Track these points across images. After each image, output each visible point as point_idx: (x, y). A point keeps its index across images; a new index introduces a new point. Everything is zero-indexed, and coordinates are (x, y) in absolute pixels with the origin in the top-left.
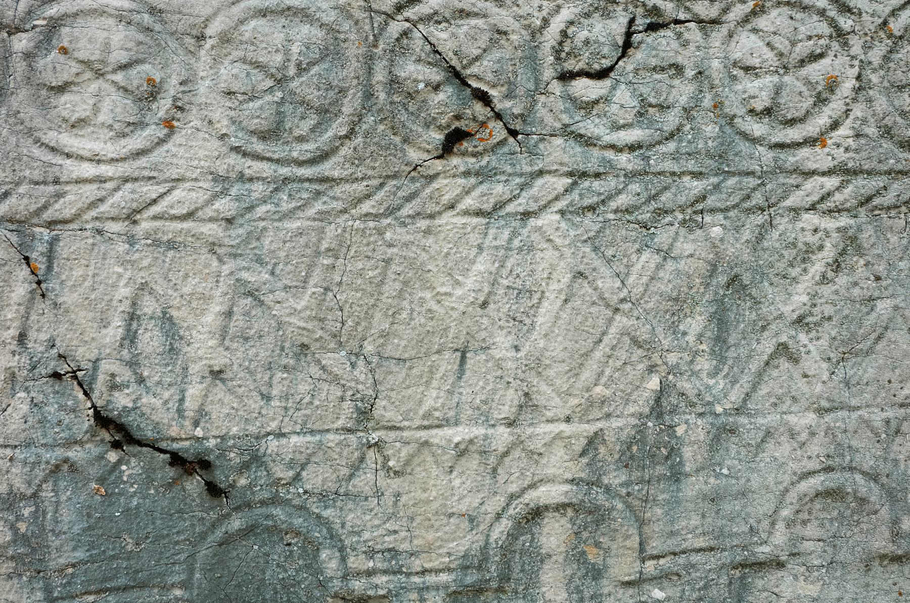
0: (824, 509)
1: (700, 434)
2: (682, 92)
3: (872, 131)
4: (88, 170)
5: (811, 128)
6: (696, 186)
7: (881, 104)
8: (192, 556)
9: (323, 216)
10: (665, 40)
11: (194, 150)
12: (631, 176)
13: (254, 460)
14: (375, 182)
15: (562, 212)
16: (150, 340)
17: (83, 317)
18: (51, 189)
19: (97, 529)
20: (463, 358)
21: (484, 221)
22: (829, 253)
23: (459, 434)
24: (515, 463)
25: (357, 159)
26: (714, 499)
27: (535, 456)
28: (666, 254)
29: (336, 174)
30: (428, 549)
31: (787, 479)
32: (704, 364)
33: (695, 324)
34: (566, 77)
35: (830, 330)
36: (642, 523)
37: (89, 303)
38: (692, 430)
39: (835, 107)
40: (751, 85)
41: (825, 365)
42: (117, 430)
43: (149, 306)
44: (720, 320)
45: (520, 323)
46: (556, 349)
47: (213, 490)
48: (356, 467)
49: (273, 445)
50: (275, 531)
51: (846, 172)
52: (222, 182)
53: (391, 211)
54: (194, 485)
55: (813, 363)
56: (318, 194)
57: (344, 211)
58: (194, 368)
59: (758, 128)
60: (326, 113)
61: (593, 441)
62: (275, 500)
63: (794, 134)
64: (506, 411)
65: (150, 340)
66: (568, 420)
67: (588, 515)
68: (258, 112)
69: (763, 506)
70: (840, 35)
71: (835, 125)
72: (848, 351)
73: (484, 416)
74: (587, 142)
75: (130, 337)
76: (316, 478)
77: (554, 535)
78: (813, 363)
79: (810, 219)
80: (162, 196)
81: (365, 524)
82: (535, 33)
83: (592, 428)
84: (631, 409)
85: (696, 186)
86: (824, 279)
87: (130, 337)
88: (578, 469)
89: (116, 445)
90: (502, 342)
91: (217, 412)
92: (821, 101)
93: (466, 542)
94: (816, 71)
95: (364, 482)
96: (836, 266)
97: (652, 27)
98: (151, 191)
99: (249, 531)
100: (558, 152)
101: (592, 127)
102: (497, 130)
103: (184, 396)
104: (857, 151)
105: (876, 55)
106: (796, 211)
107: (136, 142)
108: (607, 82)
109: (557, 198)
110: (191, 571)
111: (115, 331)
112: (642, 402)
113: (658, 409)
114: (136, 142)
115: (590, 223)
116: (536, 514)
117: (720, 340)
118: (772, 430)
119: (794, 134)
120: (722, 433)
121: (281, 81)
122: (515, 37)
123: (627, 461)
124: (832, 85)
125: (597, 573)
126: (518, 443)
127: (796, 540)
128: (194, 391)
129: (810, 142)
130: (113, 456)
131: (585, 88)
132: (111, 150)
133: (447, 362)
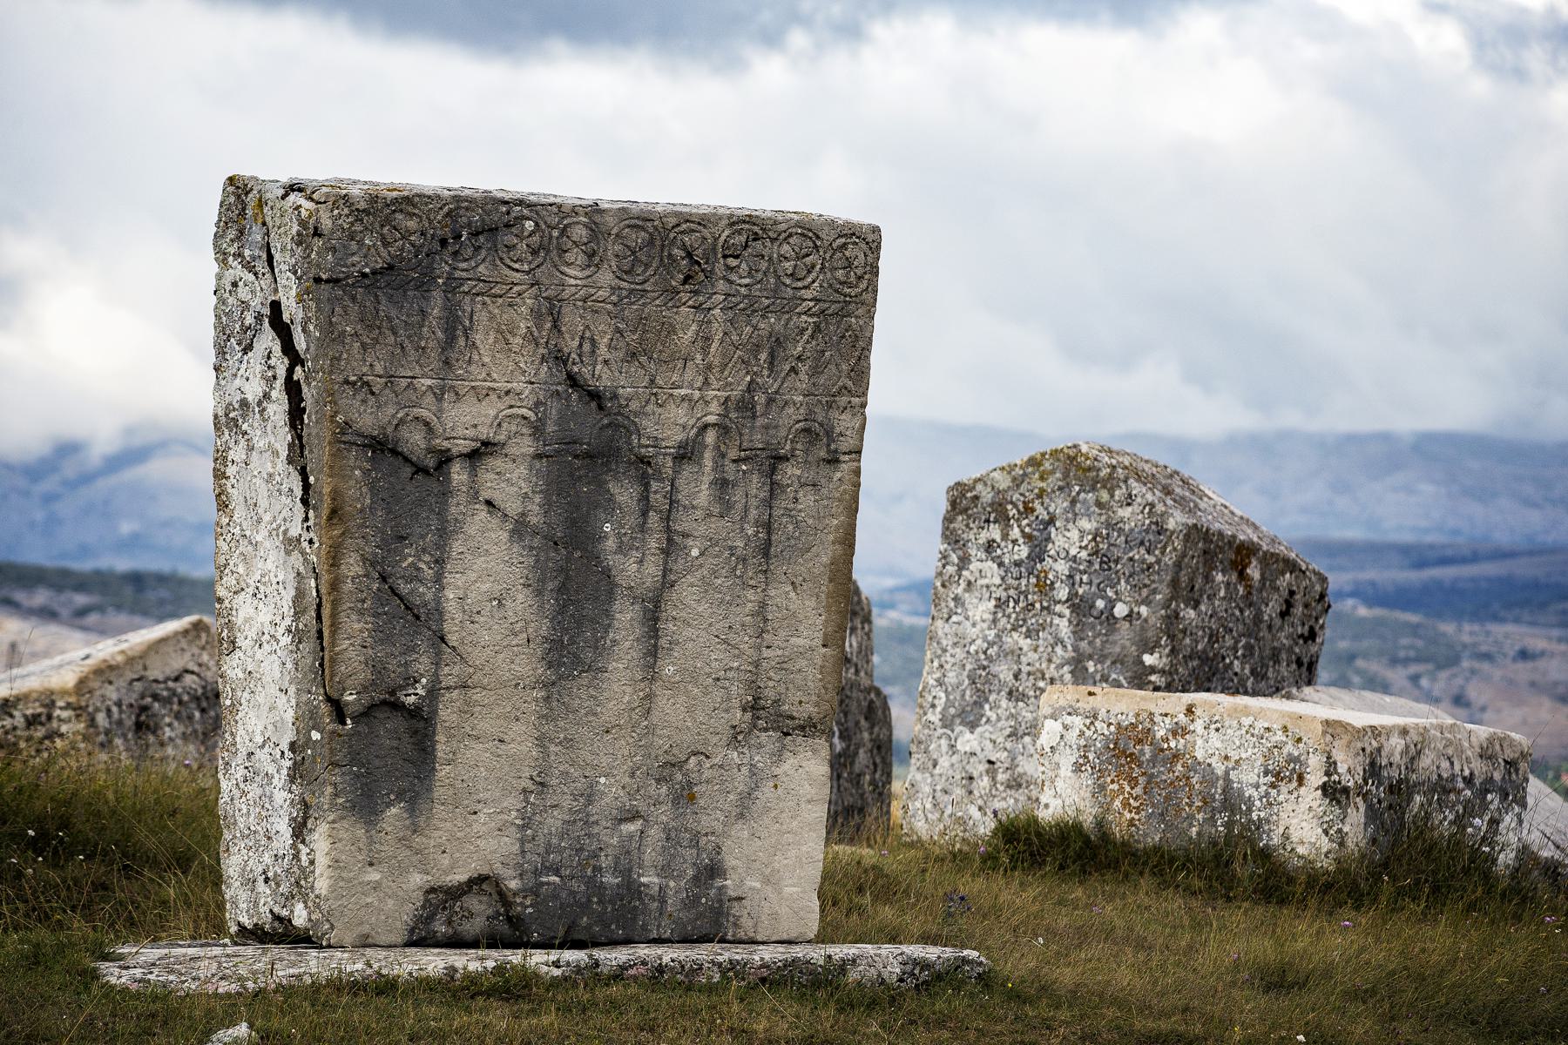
1: (763, 400)
2: (764, 265)
4: (573, 282)
5: (806, 283)
6: (767, 302)
7: (829, 275)
10: (758, 244)
12: (745, 296)
13: (615, 396)
16: (587, 347)
17: (567, 336)
19: (562, 420)
22: (809, 331)
23: (683, 392)
24: (700, 405)
25: (655, 284)
26: (766, 427)
27: (707, 403)
28: (755, 328)
30: (668, 438)
32: (766, 372)
33: (763, 356)
34: (725, 257)
35: (809, 362)
36: (741, 435)
37: (569, 332)
38: (760, 398)
39: (814, 274)
40: (787, 265)
42: (573, 381)
43: (588, 334)
44: (772, 355)
45: (705, 351)
46: (716, 362)
48: (647, 402)
49: (621, 391)
50: (618, 426)
54: (594, 405)
55: (803, 376)
59: (788, 281)
60: (647, 266)
61: (727, 399)
62: (619, 413)
63: (800, 284)
64: (699, 384)
65: (587, 347)
67: (723, 429)
68: (626, 266)
69: (783, 433)
70: (816, 247)
72: (815, 372)
73: (691, 387)
74: (731, 282)
75: (581, 345)
76: (634, 405)
77: (710, 437)
78: (803, 376)
81: (648, 425)
82: (716, 239)
85: (767, 302)
87: (581, 345)
88: (719, 410)
90: (699, 357)
91: (604, 376)
92: (809, 272)
93: (680, 437)
94: (808, 260)
95: (649, 408)
96: (812, 337)
99: (609, 425)
100: (721, 285)
101: (734, 277)
102: (701, 276)
103: (293, 426)
105: (827, 256)
107: (587, 273)
111: (576, 343)
112: (743, 387)
113: (749, 390)
114: (587, 273)
115: (730, 314)
116: (706, 426)
117: (771, 363)
118: (624, 861)
119: (800, 284)
120: (770, 401)
121: (634, 253)
123: (738, 409)
124: (813, 267)
125: (723, 456)
126: (702, 398)
127: (793, 450)
128: (599, 367)
129: (805, 287)
131: (732, 262)
132: (580, 275)
133: (680, 364)
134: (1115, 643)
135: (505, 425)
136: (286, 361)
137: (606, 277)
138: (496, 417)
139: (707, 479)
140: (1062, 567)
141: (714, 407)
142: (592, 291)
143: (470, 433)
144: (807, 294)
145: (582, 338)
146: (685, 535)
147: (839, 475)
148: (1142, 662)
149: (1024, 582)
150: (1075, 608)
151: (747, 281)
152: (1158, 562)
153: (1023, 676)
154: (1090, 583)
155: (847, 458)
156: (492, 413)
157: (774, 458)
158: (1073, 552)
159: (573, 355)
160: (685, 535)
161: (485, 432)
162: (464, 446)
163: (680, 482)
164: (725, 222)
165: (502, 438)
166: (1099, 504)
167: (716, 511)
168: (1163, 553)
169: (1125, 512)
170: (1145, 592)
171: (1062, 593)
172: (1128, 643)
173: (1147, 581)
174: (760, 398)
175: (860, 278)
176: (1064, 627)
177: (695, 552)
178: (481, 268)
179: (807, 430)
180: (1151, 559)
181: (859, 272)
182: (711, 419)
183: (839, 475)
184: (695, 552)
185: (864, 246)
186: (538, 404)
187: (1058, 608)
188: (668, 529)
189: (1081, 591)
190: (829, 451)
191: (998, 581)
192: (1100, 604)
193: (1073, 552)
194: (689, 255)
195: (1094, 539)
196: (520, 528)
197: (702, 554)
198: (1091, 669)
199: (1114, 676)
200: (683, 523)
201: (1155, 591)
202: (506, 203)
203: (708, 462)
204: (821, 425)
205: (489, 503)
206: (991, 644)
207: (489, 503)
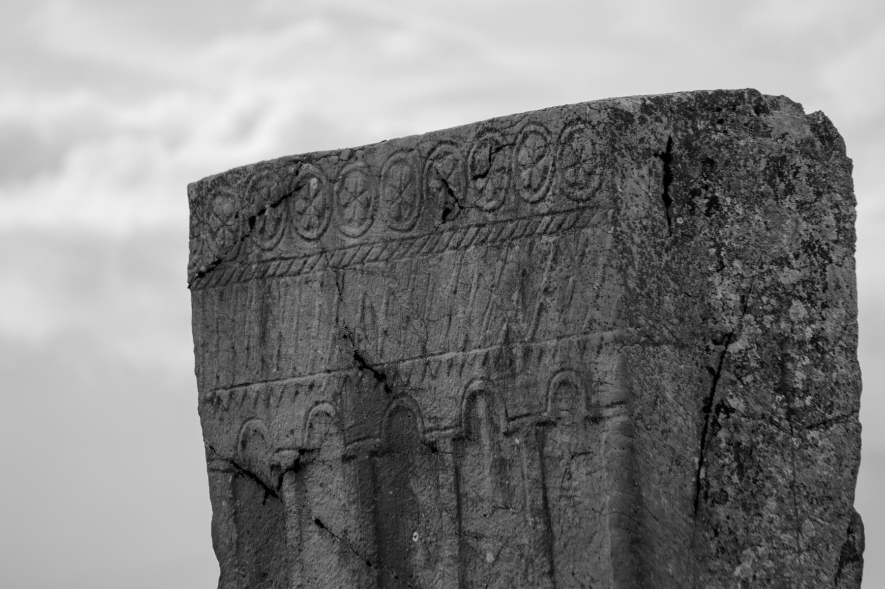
0: (566, 393)
3: (557, 191)
4: (352, 241)
8: (381, 422)
9: (412, 255)
11: (378, 230)
14: (426, 237)
15: (476, 244)
18: (342, 251)
20: (450, 319)
21: (454, 251)
25: (421, 228)
28: (505, 261)
29: (415, 235)
31: (549, 375)
32: (520, 316)
33: (515, 296)
35: (557, 295)
41: (557, 313)
43: (368, 303)
44: (522, 292)
47: (388, 390)
51: (551, 213)
52: (386, 241)
53: (431, 250)
56: (411, 244)
57: (418, 252)
58: (380, 329)
66: (480, 347)
71: (548, 190)
75: (363, 317)
79: (545, 238)
80: (370, 251)
83: (485, 351)
84: (499, 341)
86: (552, 269)
87: (363, 317)
89: (361, 368)
97: (498, 150)
98: (366, 248)
104: (554, 202)
106: (540, 234)
108: (485, 179)
109: (474, 238)
110: (381, 428)
114: (363, 228)
120: (527, 352)
122: (751, 300)
127: (557, 410)
130: (360, 374)
135: (316, 426)
136: (662, 163)
137: (378, 230)
138: (306, 418)
139: (487, 461)
141: (477, 370)
142: (366, 248)
143: (289, 441)
144: (543, 207)
145: (364, 308)
146: (478, 537)
147: (604, 436)
151: (491, 205)
155: (609, 412)
156: (302, 413)
157: (539, 424)
159: (358, 331)
160: (478, 537)
161: (300, 438)
162: (287, 457)
163: (465, 470)
164: (473, 134)
165: (315, 442)
167: (500, 501)
174: (518, 350)
175: (590, 174)
177: (490, 558)
178: (281, 246)
179: (564, 383)
181: (587, 166)
182: (476, 385)
183: (604, 436)
184: (490, 558)
185: (588, 131)
186: (336, 395)
188: (460, 532)
190: (589, 407)
194: (445, 183)
196: (346, 551)
197: (497, 558)
200: (474, 523)
202: (296, 161)
203: (486, 441)
204: (578, 373)
205: (318, 522)
207: (318, 522)
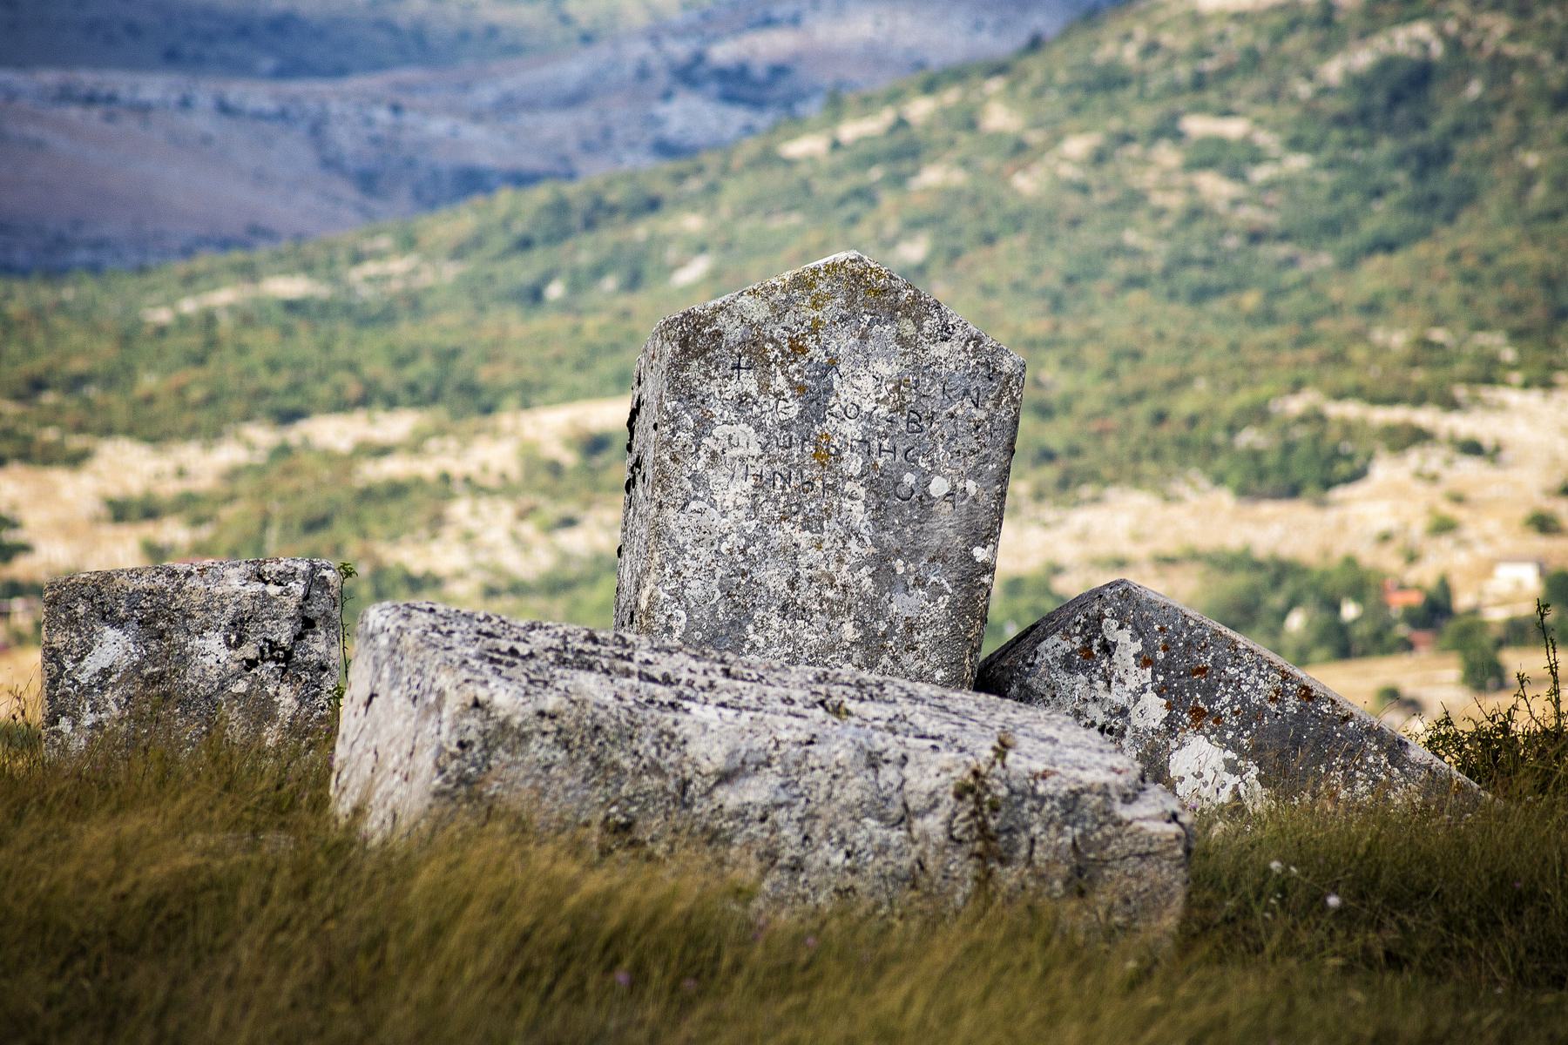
134: (932, 531)
140: (852, 429)
148: (972, 558)
149: (796, 451)
150: (873, 486)
152: (991, 418)
153: (803, 583)
154: (894, 451)
158: (867, 407)
166: (901, 340)
168: (996, 406)
169: (941, 350)
170: (972, 461)
171: (854, 464)
172: (950, 533)
173: (975, 446)
176: (858, 513)
180: (981, 415)
187: (849, 487)
189: (881, 462)
191: (757, 451)
192: (909, 479)
193: (867, 407)
195: (897, 388)
198: (901, 571)
199: (933, 579)
201: (986, 459)
206: (751, 540)
